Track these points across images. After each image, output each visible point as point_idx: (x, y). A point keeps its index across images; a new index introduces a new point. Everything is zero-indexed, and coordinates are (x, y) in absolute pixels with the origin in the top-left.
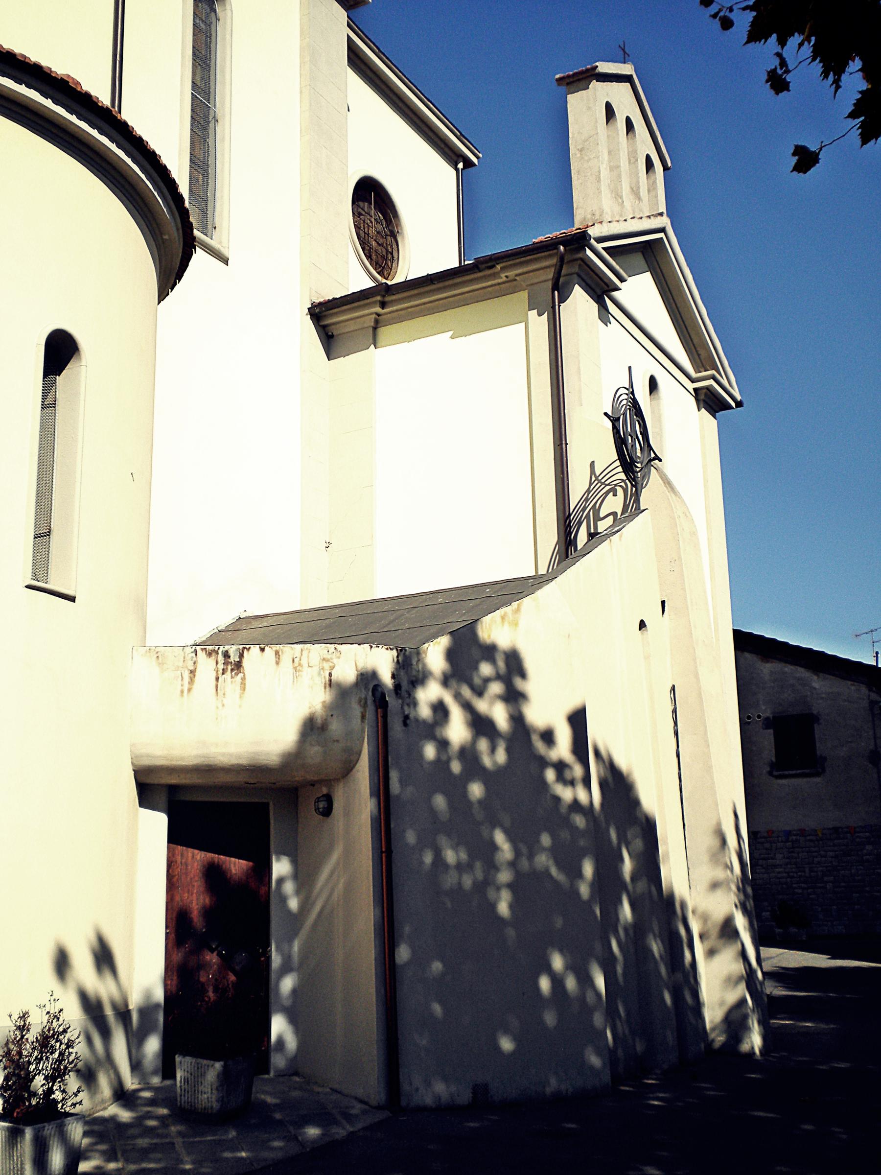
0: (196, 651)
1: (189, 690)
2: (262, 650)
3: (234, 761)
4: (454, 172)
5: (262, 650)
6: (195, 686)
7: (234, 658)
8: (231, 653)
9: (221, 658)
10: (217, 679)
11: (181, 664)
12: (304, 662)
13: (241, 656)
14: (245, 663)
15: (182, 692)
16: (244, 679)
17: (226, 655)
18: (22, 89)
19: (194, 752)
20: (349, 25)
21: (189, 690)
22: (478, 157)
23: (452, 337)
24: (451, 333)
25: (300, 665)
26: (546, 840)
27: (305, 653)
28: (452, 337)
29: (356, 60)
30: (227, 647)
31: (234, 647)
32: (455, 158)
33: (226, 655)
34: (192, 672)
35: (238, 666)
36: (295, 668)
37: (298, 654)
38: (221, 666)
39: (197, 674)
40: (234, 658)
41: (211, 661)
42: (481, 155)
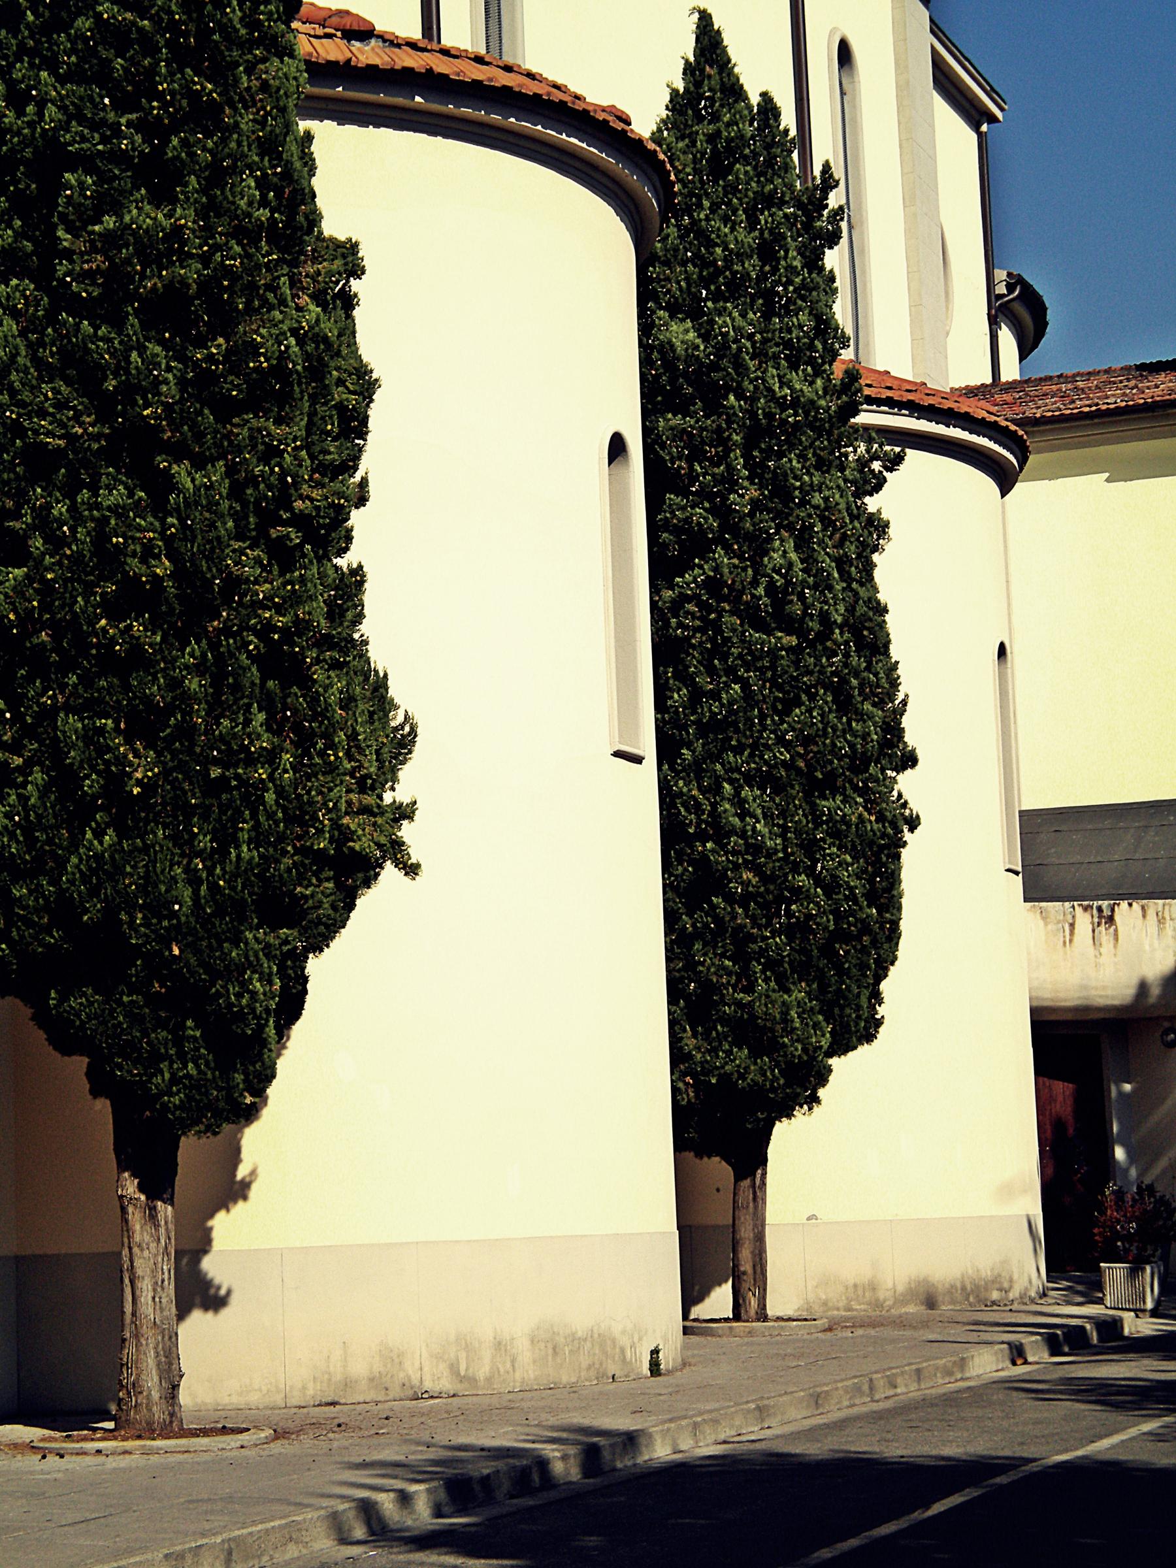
0: (1073, 907)
1: (1071, 941)
2: (1130, 905)
3: (1109, 1002)
4: (975, 136)
5: (1130, 905)
6: (1076, 938)
7: (1107, 912)
8: (1104, 907)
9: (1095, 912)
10: (1094, 931)
11: (1061, 917)
12: (1167, 916)
13: (1113, 910)
14: (1117, 917)
15: (1065, 943)
16: (1116, 930)
17: (1100, 909)
18: (974, 438)
19: (1077, 995)
20: (932, 31)
21: (1071, 941)
22: (1002, 109)
23: (1108, 480)
24: (1107, 475)
25: (1163, 918)
26: (37, 834)
27: (1167, 908)
28: (1108, 480)
29: (945, 82)
30: (1100, 902)
31: (1106, 903)
32: (977, 117)
33: (1100, 909)
34: (1072, 925)
35: (1111, 920)
36: (1159, 921)
37: (1160, 909)
38: (1096, 920)
39: (1076, 926)
40: (1107, 912)
41: (1087, 916)
42: (1006, 107)
